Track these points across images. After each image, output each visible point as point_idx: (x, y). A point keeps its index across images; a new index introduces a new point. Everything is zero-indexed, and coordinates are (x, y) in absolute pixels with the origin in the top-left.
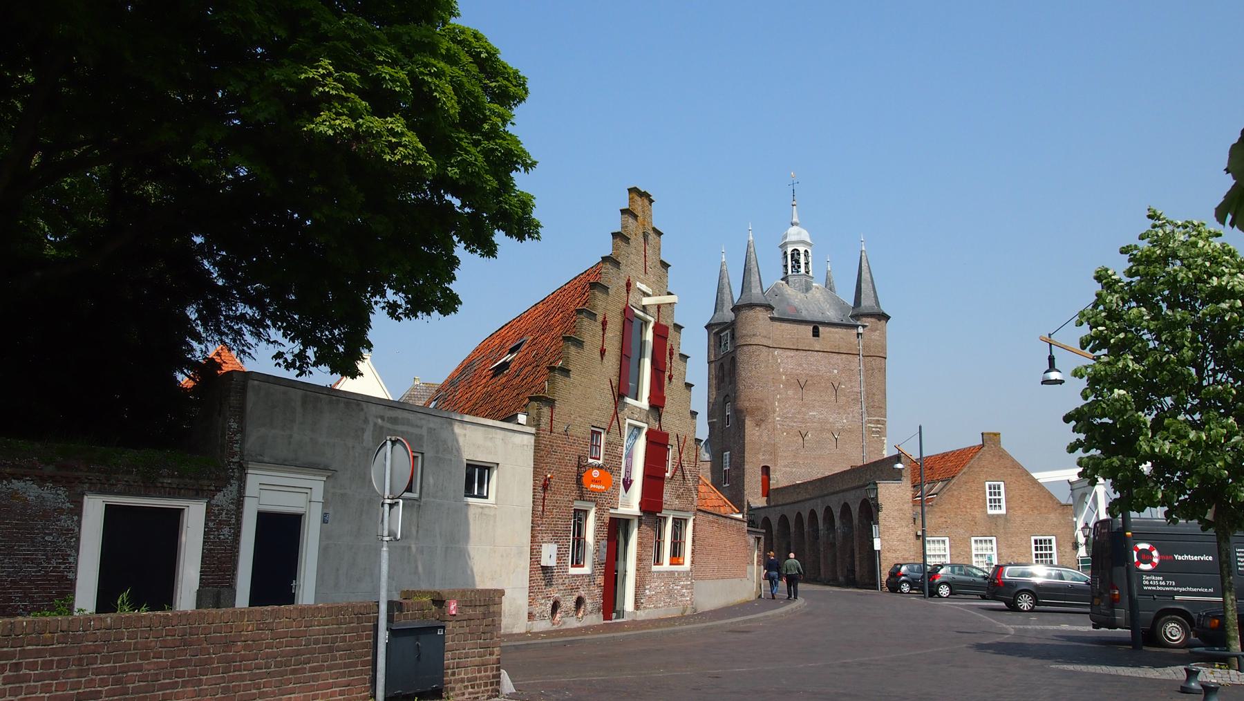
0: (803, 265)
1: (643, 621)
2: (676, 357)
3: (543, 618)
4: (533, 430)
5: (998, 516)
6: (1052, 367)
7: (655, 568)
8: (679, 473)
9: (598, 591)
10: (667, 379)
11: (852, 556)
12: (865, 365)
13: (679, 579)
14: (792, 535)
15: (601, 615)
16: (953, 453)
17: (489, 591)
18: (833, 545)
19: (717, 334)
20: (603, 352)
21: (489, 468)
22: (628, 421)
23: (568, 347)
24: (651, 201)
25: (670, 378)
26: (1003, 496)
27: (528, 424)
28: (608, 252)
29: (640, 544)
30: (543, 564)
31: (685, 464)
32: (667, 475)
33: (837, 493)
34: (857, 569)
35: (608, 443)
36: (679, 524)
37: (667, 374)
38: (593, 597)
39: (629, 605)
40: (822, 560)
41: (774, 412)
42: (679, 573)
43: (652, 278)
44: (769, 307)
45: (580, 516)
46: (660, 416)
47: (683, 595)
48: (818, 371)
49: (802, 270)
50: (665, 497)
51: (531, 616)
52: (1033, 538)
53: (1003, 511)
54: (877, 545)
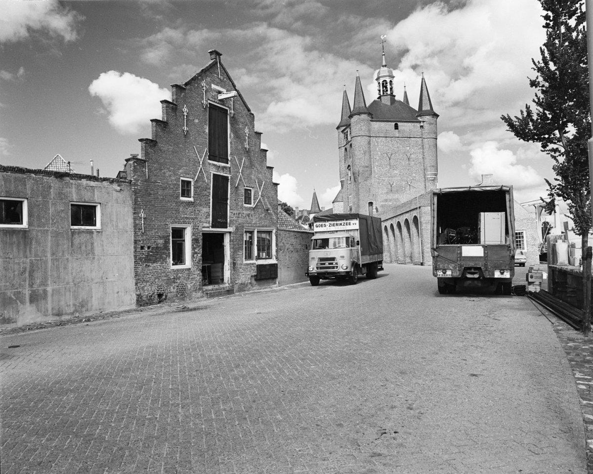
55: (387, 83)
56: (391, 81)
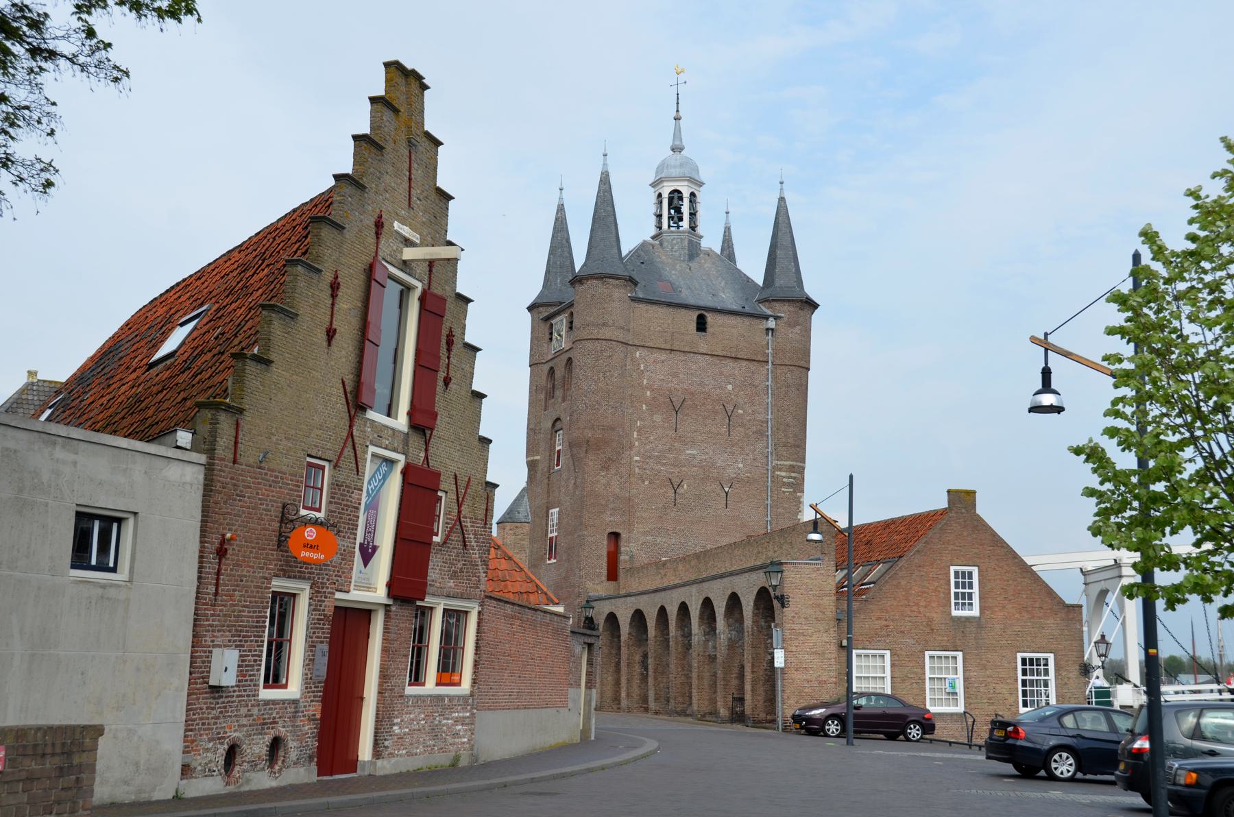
0: (686, 216)
1: (385, 776)
2: (457, 348)
3: (209, 773)
4: (203, 459)
5: (968, 619)
6: (1047, 387)
7: (411, 690)
8: (456, 537)
9: (309, 728)
10: (440, 383)
11: (741, 676)
12: (775, 378)
13: (451, 708)
14: (651, 642)
15: (314, 767)
16: (903, 520)
17: (73, 728)
18: (713, 659)
19: (548, 319)
20: (331, 334)
21: (120, 521)
22: (372, 449)
23: (270, 322)
24: (425, 87)
25: (447, 381)
26: (976, 590)
27: (195, 448)
28: (347, 167)
29: (385, 650)
30: (213, 682)
31: (467, 523)
32: (436, 539)
33: (721, 576)
34: (748, 696)
35: (335, 485)
36: (454, 618)
37: (442, 375)
38: (301, 739)
39: (365, 751)
40: (695, 682)
41: (631, 447)
42: (451, 698)
43: (421, 217)
44: (633, 282)
45: (282, 605)
46: (427, 444)
47: (456, 735)
48: (702, 384)
49: (685, 224)
50: (432, 575)
51: (186, 770)
52: (1020, 656)
53: (975, 612)
54: (779, 659)
55: (681, 199)
56: (693, 195)
